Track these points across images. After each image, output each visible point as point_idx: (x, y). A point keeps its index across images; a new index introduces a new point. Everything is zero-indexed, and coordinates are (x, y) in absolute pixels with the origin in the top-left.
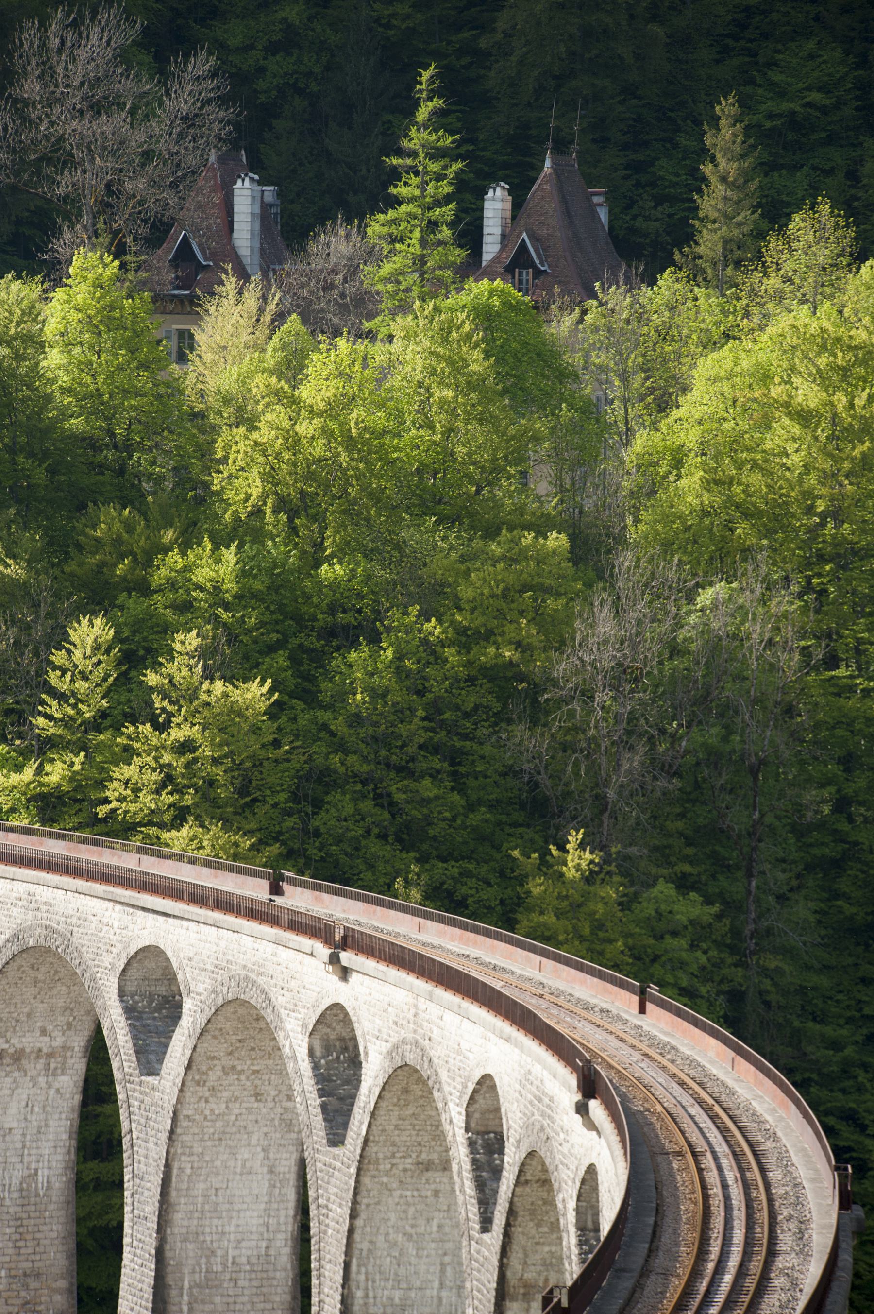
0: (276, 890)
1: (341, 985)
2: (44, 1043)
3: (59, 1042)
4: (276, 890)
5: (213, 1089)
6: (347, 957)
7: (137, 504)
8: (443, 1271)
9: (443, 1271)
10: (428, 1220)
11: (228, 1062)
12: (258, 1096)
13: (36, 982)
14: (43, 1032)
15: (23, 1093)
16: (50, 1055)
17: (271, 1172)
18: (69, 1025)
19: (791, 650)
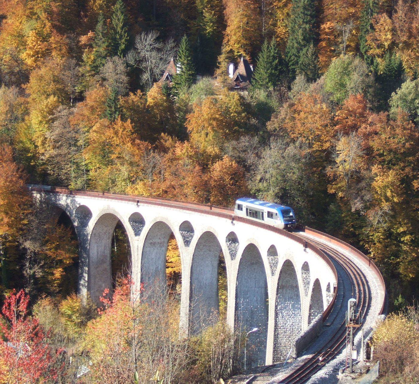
0: (211, 209)
1: (134, 236)
2: (159, 241)
3: (162, 240)
4: (211, 209)
5: (201, 249)
6: (234, 222)
7: (399, 205)
8: (255, 284)
9: (255, 284)
10: (253, 274)
11: (204, 244)
12: (210, 251)
13: (158, 228)
14: (159, 239)
15: (155, 251)
16: (161, 243)
17: (212, 266)
18: (165, 237)
19: (327, 131)
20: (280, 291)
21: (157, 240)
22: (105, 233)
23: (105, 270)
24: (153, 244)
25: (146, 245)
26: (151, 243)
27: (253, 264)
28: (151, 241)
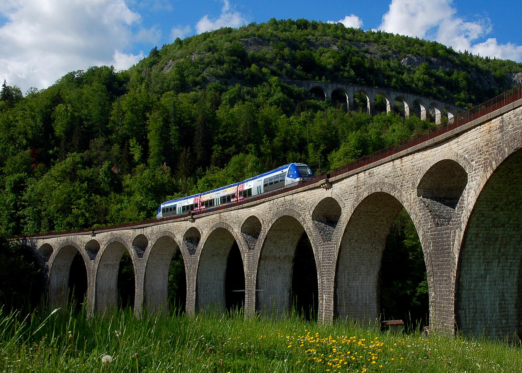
12: (162, 259)
20: (262, 262)
22: (64, 266)
24: (107, 266)
26: (105, 265)
27: (213, 255)
28: (105, 263)
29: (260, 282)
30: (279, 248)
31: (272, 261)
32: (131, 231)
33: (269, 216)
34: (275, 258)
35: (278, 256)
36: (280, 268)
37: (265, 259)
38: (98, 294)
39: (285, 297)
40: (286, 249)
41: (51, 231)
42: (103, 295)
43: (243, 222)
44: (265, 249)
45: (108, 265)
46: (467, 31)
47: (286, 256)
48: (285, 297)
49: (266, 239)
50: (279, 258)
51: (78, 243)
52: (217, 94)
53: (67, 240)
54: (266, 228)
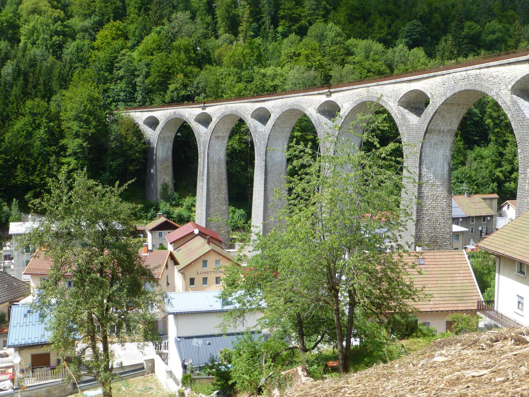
12: (283, 132)
20: (428, 135)
21: (220, 134)
23: (168, 166)
24: (217, 137)
25: (212, 137)
26: (216, 137)
29: (423, 155)
30: (445, 122)
31: (436, 135)
32: (249, 105)
33: (163, 118)
34: (439, 131)
35: (442, 129)
36: (442, 141)
37: (431, 133)
38: (210, 164)
39: (445, 170)
40: (451, 123)
41: (143, 105)
42: (214, 166)
43: (401, 96)
44: (432, 123)
45: (218, 137)
46: (5, 82)
47: (449, 130)
48: (445, 170)
49: (436, 112)
50: (443, 131)
51: (187, 115)
52: (96, 47)
53: (175, 113)
54: (215, 120)
